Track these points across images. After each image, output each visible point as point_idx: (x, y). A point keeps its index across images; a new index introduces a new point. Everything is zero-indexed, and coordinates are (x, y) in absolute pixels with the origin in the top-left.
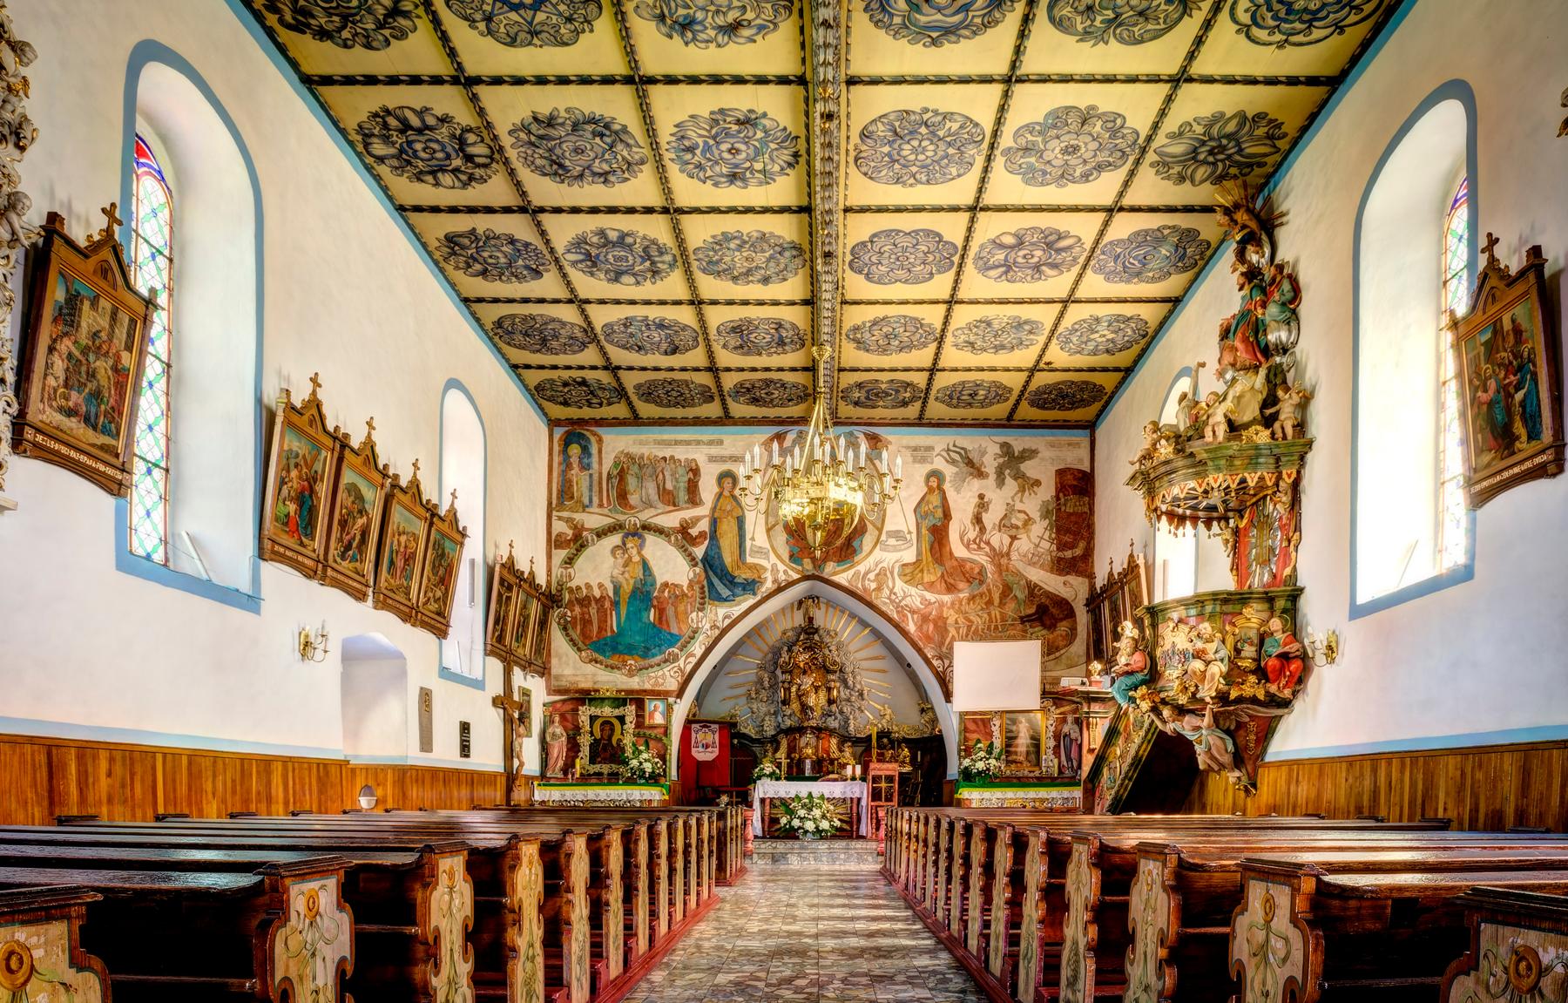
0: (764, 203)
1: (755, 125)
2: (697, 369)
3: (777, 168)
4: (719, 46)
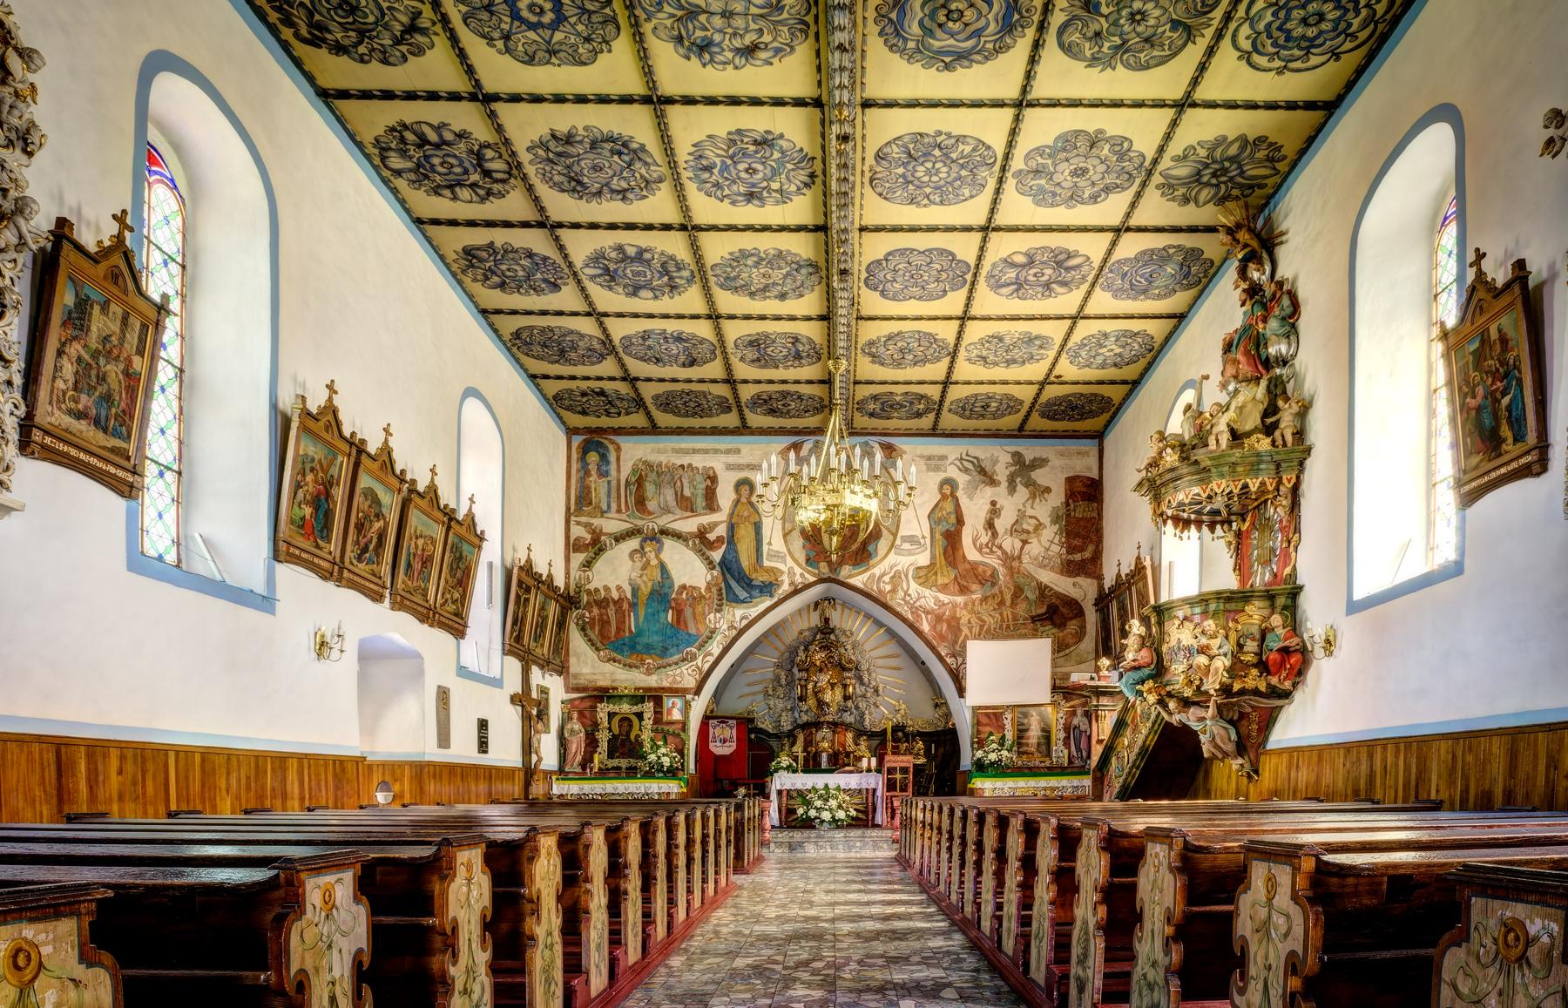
0: (781, 222)
1: (771, 146)
2: (714, 381)
4: (736, 68)
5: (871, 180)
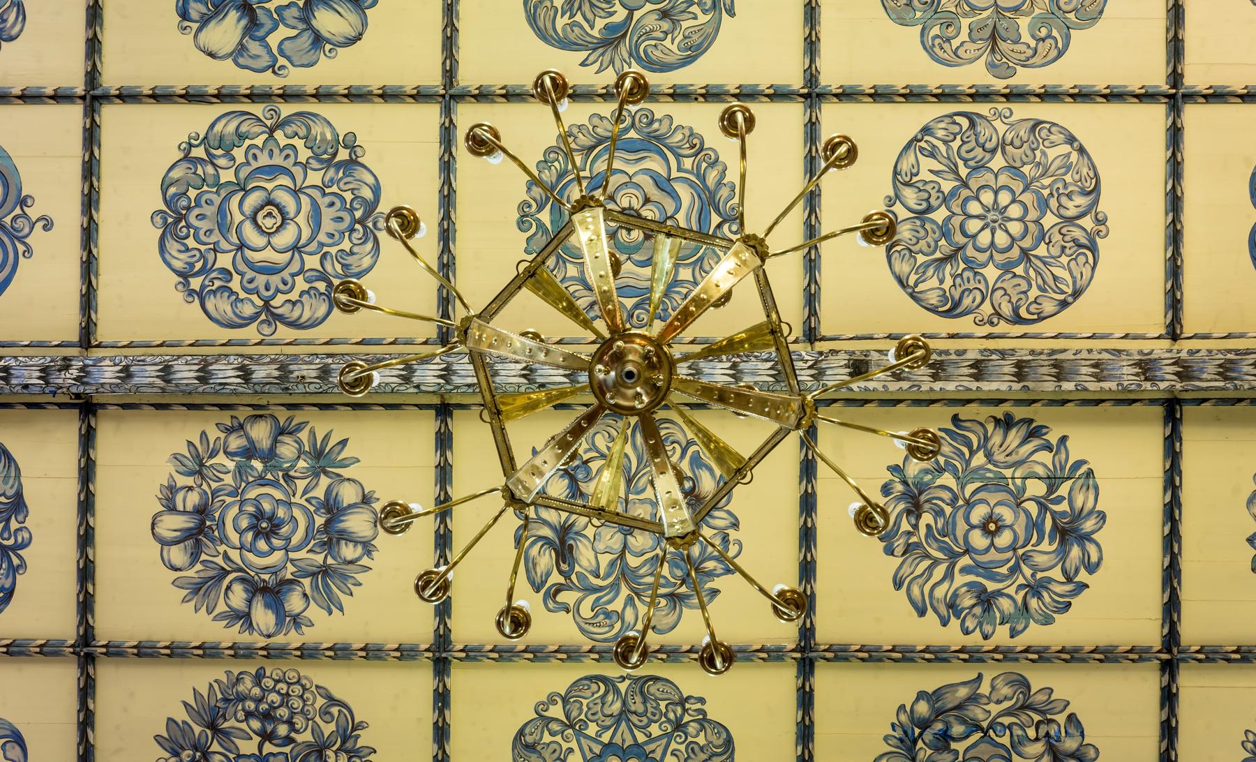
0: (1158, 484)
1: (922, 488)
3: (1045, 457)
4: (735, 525)
5: (1018, 320)
